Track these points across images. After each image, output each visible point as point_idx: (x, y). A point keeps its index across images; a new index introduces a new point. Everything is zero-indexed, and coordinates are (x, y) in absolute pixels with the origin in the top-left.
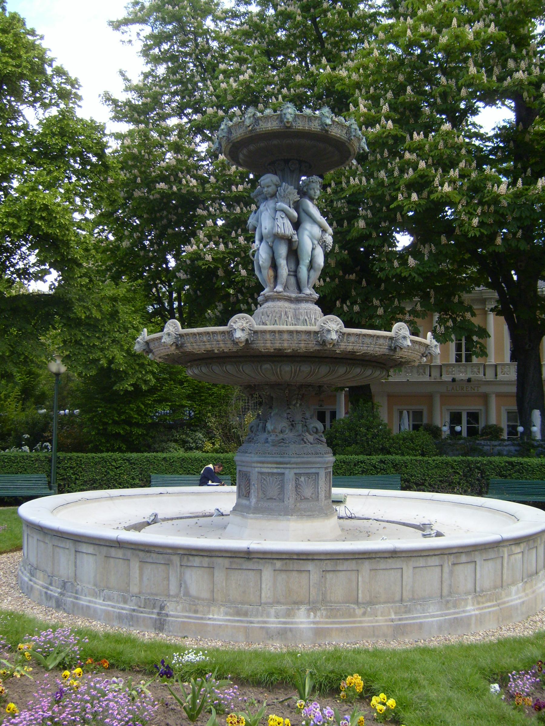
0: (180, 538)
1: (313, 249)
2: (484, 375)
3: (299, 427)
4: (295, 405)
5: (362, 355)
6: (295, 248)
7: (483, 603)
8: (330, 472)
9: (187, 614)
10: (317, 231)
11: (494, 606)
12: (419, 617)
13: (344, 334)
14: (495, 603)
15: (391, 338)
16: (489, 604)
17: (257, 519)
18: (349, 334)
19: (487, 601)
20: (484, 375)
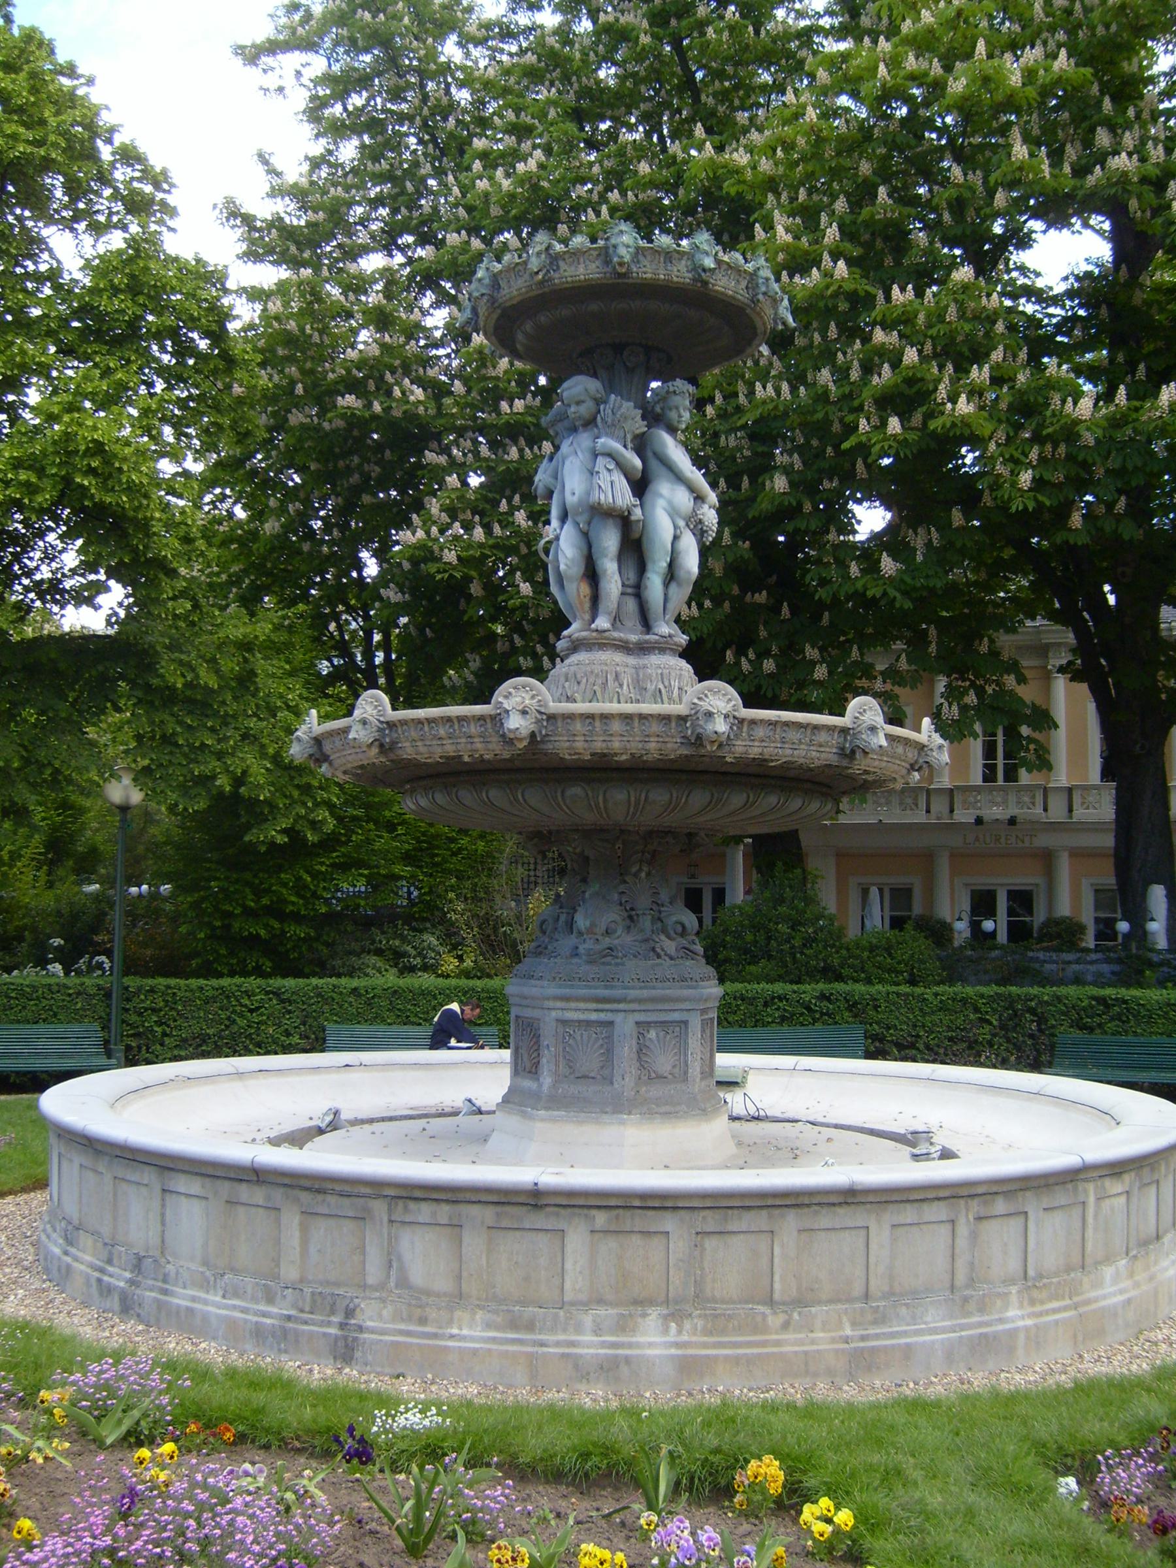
1: (676, 538)
2: (1045, 810)
3: (646, 923)
4: (636, 875)
5: (781, 766)
6: (636, 535)
7: (1042, 1302)
8: (712, 1019)
9: (402, 1326)
10: (683, 499)
11: (1065, 1308)
13: (741, 721)
14: (1067, 1302)
16: (1055, 1304)
18: (753, 722)
19: (1051, 1298)
20: (1045, 810)
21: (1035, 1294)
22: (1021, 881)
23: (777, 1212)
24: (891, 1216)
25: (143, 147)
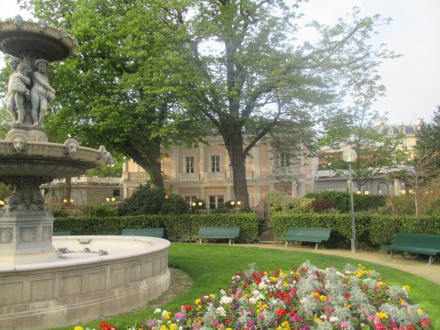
0: (63, 262)
1: (40, 101)
2: (253, 177)
3: (28, 201)
4: (26, 188)
5: (82, 161)
6: (28, 100)
7: (88, 300)
8: (51, 226)
9: (93, 301)
10: (41, 89)
11: (98, 301)
12: (77, 305)
13: (78, 149)
14: (99, 299)
15: (64, 148)
16: (93, 301)
17: (408, 264)
18: (81, 149)
19: (92, 299)
20: (253, 177)
21: (86, 298)
22: (220, 194)
23: (27, 276)
24: (31, 278)
25: (391, 59)
